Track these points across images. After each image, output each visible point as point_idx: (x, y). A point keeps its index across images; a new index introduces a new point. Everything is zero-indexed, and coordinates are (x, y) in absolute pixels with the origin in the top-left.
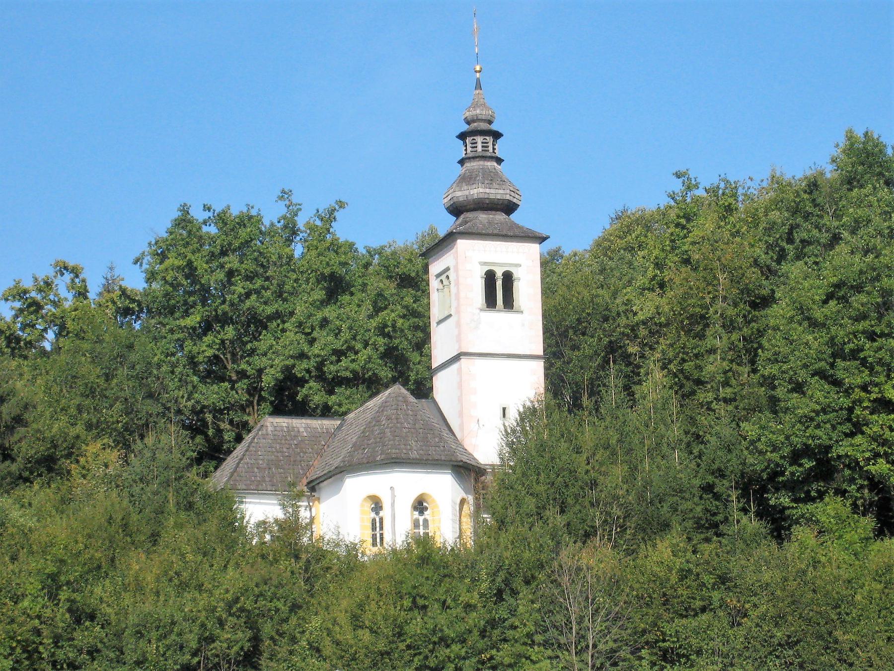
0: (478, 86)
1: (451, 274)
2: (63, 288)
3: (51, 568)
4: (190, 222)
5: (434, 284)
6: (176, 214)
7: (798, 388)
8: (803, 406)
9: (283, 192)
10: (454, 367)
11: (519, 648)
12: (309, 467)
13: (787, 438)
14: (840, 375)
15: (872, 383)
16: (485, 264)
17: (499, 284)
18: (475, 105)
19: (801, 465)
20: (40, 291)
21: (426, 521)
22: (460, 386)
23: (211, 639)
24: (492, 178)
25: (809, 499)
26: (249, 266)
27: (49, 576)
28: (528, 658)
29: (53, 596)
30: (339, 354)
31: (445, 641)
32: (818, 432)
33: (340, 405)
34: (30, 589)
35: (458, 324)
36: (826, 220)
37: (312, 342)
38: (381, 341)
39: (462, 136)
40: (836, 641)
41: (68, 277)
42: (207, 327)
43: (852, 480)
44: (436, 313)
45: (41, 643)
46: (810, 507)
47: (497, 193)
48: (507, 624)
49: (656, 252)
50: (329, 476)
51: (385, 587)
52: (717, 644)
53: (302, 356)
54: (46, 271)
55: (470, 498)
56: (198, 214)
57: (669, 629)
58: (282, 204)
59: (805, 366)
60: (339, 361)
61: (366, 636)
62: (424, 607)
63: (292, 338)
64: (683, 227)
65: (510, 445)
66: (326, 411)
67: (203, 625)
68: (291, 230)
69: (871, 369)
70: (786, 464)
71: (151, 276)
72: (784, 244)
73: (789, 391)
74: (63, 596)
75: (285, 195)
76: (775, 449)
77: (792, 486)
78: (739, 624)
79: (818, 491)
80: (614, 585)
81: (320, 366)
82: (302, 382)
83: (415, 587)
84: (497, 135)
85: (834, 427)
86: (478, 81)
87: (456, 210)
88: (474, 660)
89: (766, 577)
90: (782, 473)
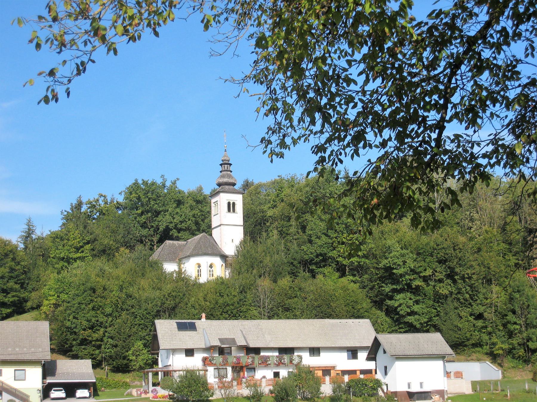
0: (225, 151)
1: (218, 202)
2: (101, 202)
3: (121, 283)
4: (138, 184)
5: (213, 205)
6: (134, 182)
7: (319, 238)
8: (319, 242)
9: (162, 175)
10: (219, 228)
11: (248, 307)
12: (179, 254)
13: (315, 251)
14: (329, 234)
15: (338, 236)
16: (228, 200)
17: (231, 205)
18: (225, 156)
19: (319, 258)
20: (96, 202)
21: (212, 270)
22: (221, 233)
23: (164, 304)
24: (230, 176)
25: (320, 267)
26: (154, 196)
27: (120, 285)
28: (250, 310)
29: (121, 291)
30: (181, 222)
31: (228, 305)
32: (324, 249)
33: (182, 236)
34: (115, 289)
35: (220, 217)
36: (322, 190)
37: (174, 218)
38: (194, 219)
39: (221, 165)
40: (331, 306)
41: (102, 198)
42: (142, 213)
43: (332, 263)
44: (213, 212)
45: (118, 304)
46: (321, 269)
47: (231, 181)
48: (243, 300)
49: (273, 198)
50: (185, 257)
51: (212, 290)
52: (299, 306)
53: (171, 223)
54: (97, 197)
55: (224, 264)
56: (140, 182)
57: (286, 302)
58: (162, 179)
59: (320, 232)
60: (181, 224)
61: (208, 303)
62: (223, 296)
63: (168, 217)
64: (280, 191)
65: (237, 250)
66: (178, 239)
67: (162, 300)
68: (164, 186)
69: (338, 233)
70: (315, 258)
71: (126, 198)
72: (310, 197)
73: (315, 238)
74: (124, 291)
75: (162, 176)
76: (312, 253)
77: (316, 264)
78: (305, 301)
79: (323, 265)
80: (272, 290)
81: (176, 225)
82: (172, 230)
83: (220, 290)
84: (230, 165)
85: (328, 248)
86: (225, 150)
87: (219, 185)
88: (236, 310)
89: (312, 289)
90: (314, 260)
